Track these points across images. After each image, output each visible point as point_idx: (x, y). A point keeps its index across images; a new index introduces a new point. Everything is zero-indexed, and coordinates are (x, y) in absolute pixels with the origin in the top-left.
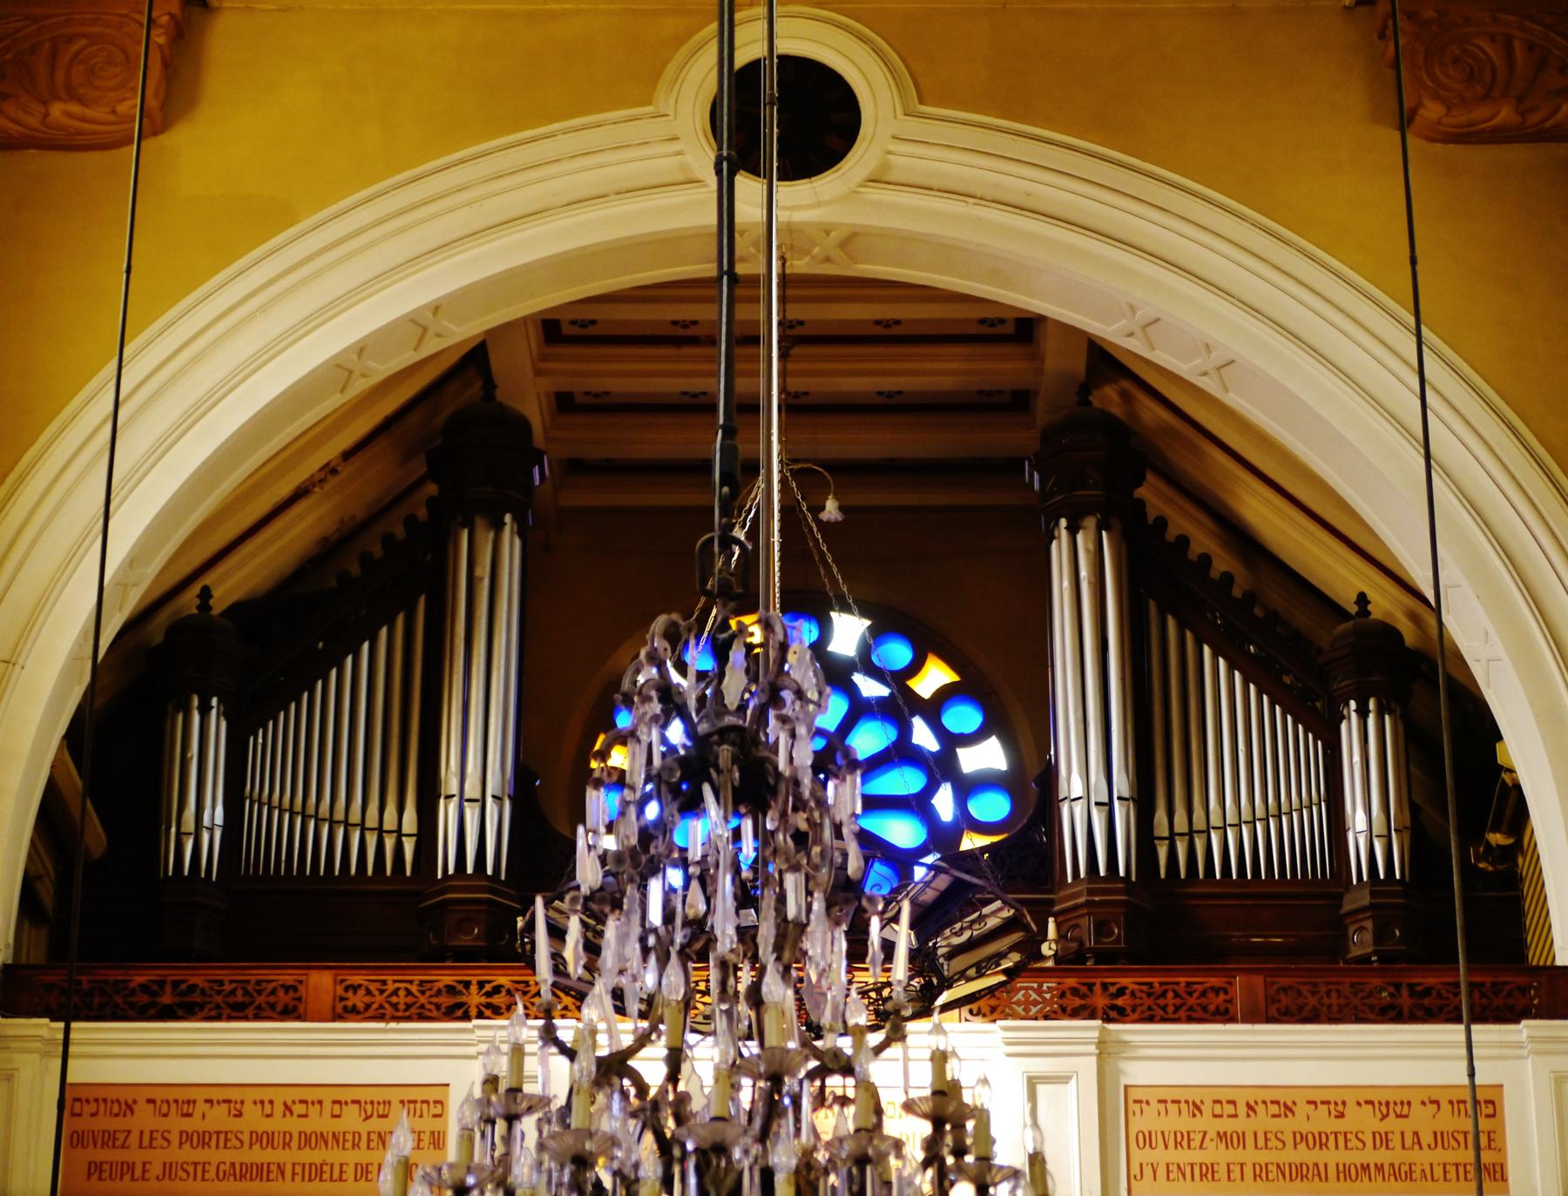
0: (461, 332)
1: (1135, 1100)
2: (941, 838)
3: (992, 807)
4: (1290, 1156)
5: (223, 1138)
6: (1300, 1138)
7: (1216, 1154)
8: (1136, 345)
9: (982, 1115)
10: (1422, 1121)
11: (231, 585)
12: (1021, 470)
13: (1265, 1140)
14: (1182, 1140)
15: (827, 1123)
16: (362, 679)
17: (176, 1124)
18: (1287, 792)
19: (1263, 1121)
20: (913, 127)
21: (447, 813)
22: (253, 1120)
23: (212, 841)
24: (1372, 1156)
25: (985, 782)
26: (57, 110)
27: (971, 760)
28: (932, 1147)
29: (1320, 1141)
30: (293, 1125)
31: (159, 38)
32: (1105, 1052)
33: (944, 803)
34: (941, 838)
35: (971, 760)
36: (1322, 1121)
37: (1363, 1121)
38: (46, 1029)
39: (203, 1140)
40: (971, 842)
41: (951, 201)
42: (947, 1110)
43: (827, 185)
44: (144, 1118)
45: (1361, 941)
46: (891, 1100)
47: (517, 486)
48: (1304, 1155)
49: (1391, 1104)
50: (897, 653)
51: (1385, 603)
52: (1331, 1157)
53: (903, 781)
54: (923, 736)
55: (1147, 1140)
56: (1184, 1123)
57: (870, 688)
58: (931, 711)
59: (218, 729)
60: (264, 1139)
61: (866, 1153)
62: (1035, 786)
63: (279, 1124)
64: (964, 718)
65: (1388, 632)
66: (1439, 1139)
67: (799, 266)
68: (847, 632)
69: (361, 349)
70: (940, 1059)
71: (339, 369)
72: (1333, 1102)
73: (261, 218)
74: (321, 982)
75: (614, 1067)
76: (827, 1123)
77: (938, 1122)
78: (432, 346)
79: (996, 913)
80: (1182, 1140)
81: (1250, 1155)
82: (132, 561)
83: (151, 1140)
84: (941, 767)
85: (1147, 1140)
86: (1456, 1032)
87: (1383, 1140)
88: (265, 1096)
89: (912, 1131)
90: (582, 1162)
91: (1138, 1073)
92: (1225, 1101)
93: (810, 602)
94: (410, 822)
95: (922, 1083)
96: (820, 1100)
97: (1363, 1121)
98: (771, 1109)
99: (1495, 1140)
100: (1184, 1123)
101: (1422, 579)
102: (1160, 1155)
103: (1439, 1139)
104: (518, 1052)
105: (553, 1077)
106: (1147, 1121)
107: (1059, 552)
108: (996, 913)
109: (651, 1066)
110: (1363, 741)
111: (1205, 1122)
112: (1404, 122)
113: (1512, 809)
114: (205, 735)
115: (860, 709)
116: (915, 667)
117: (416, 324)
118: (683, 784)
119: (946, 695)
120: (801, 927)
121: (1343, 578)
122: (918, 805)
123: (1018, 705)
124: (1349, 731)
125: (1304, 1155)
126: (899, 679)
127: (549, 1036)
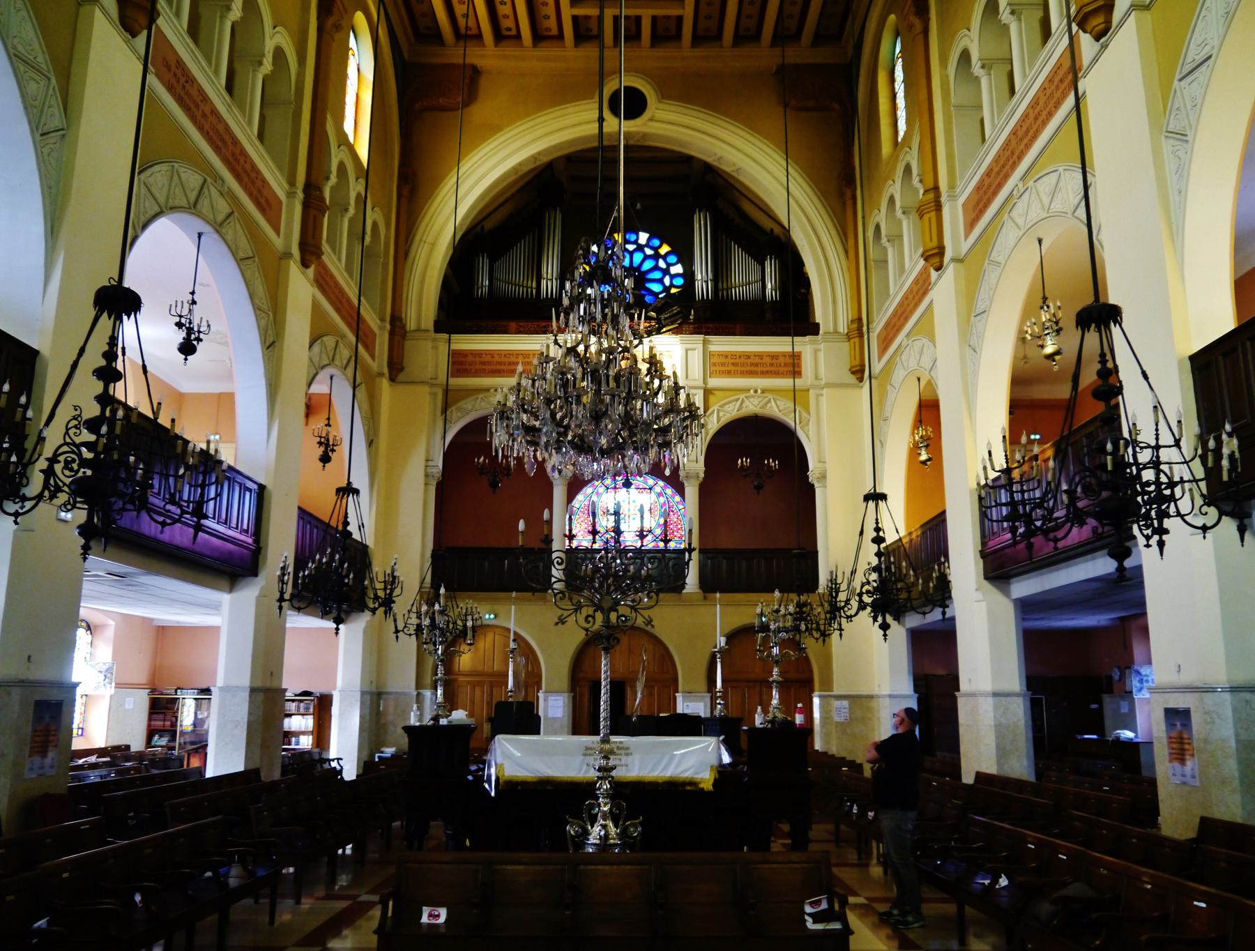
0: (545, 159)
1: (712, 354)
2: (666, 289)
3: (679, 281)
4: (748, 369)
5: (489, 363)
6: (752, 364)
7: (731, 368)
8: (716, 164)
9: (661, 363)
10: (781, 360)
11: (489, 225)
12: (686, 195)
13: (743, 365)
14: (723, 364)
15: (624, 364)
16: (520, 253)
17: (478, 359)
18: (754, 279)
19: (743, 360)
20: (661, 106)
21: (544, 283)
22: (497, 358)
23: (485, 290)
24: (769, 369)
25: (677, 275)
26: (441, 100)
27: (674, 270)
28: (649, 370)
29: (757, 365)
30: (507, 360)
31: (467, 81)
32: (705, 342)
33: (667, 281)
34: (666, 289)
35: (674, 270)
36: (757, 360)
37: (767, 360)
38: (446, 336)
39: (484, 363)
40: (673, 291)
41: (672, 124)
42: (653, 362)
43: (639, 121)
44: (470, 358)
45: (768, 316)
46: (639, 358)
47: (557, 200)
48: (753, 368)
49: (774, 356)
50: (656, 242)
51: (777, 230)
52: (759, 369)
53: (657, 275)
54: (662, 264)
55: (715, 364)
56: (723, 360)
57: (649, 252)
58: (664, 257)
59: (486, 261)
60: (500, 363)
61: (633, 371)
62: (689, 276)
63: (503, 359)
64: (672, 259)
65: (778, 238)
66: (786, 365)
67: (631, 142)
68: (643, 237)
69: (539, 153)
70: (651, 349)
71: (514, 170)
72: (760, 355)
73: (493, 129)
74: (513, 325)
75: (572, 351)
76: (624, 364)
77: (651, 363)
78: (538, 163)
79: (676, 309)
80: (723, 364)
81: (739, 368)
82: (464, 219)
83: (472, 363)
84: (666, 272)
85: (715, 364)
86: (789, 339)
87: (772, 365)
88: (499, 353)
89: (644, 367)
90: (563, 374)
91: (712, 348)
92: (734, 355)
93: (632, 228)
94: (534, 285)
95: (647, 356)
96: (623, 358)
97: (767, 360)
98: (609, 361)
99: (799, 365)
100: (723, 360)
101: (786, 225)
102: (718, 368)
103: (786, 365)
104: (548, 346)
105: (555, 352)
106: (715, 360)
107: (696, 217)
108: (676, 309)
109: (581, 348)
110: (770, 267)
111: (729, 360)
112: (786, 105)
113: (806, 283)
114: (484, 264)
115: (646, 257)
116: (660, 246)
117: (534, 158)
118: (588, 280)
119: (668, 254)
120: (618, 316)
121: (767, 224)
122: (660, 281)
123: (686, 257)
124: (767, 264)
125: (753, 368)
126: (656, 249)
127: (556, 342)
